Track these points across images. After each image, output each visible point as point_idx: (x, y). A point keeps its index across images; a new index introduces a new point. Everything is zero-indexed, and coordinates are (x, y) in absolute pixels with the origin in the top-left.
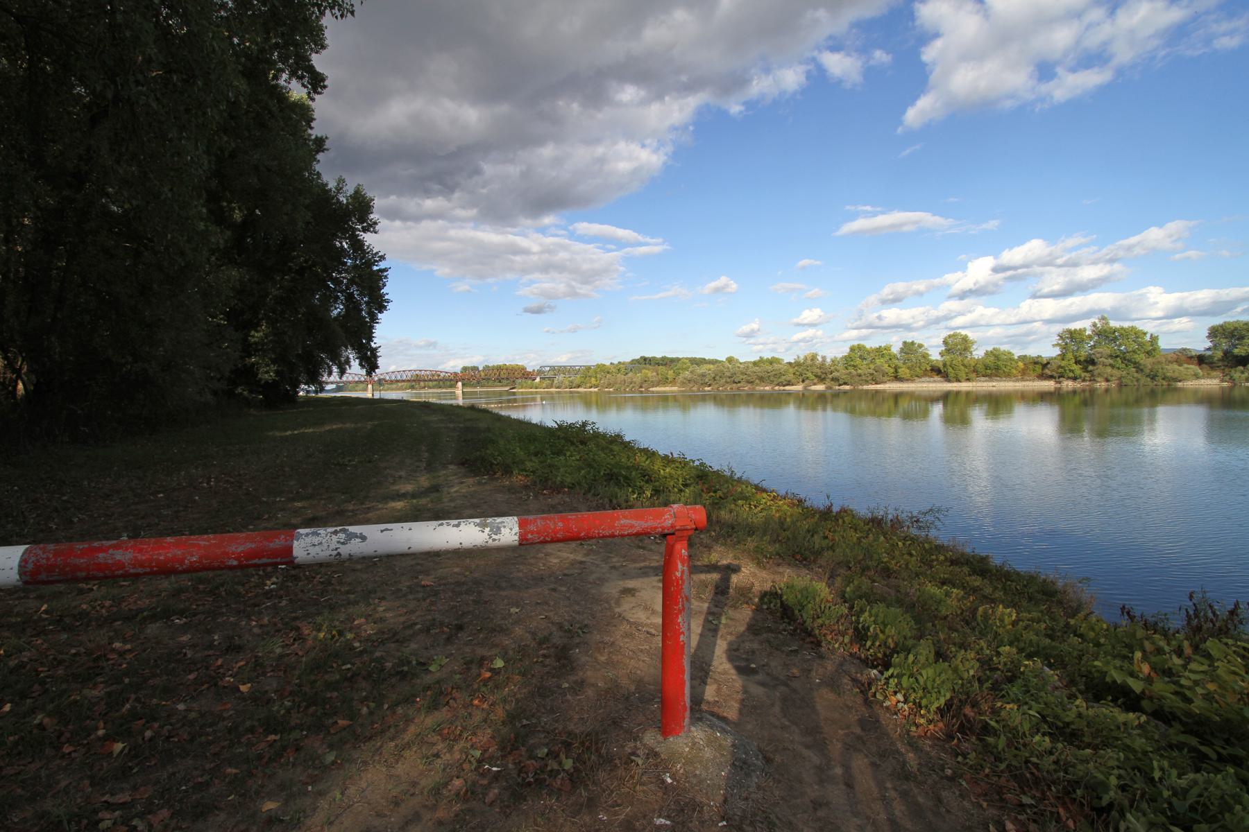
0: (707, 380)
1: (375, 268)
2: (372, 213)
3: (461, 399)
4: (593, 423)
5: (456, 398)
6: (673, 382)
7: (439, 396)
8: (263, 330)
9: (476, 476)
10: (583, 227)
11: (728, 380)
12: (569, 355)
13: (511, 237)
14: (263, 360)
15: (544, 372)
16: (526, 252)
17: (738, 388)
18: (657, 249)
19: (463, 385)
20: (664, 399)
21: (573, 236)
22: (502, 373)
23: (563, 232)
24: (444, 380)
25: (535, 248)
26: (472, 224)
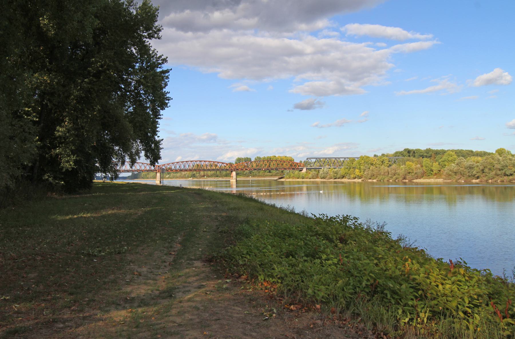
0: (474, 173)
1: (159, 70)
2: (156, 21)
3: (234, 186)
4: (355, 218)
5: (230, 186)
6: (438, 174)
7: (216, 184)
8: (66, 126)
9: (218, 278)
10: (354, 28)
11: (499, 172)
12: (336, 148)
13: (287, 41)
14: (65, 151)
15: (310, 163)
16: (300, 53)
17: (510, 181)
18: (427, 45)
19: (237, 174)
20: (428, 190)
21: (343, 36)
22: (272, 164)
23: (335, 33)
24: (221, 170)
25: (309, 49)
26: (253, 31)
